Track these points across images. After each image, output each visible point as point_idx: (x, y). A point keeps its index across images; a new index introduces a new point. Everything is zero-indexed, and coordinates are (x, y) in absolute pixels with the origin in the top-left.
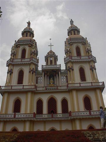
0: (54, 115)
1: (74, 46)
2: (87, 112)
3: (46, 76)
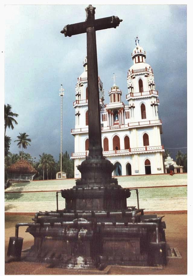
0: (118, 151)
1: (137, 78)
2: (144, 148)
3: (110, 114)
